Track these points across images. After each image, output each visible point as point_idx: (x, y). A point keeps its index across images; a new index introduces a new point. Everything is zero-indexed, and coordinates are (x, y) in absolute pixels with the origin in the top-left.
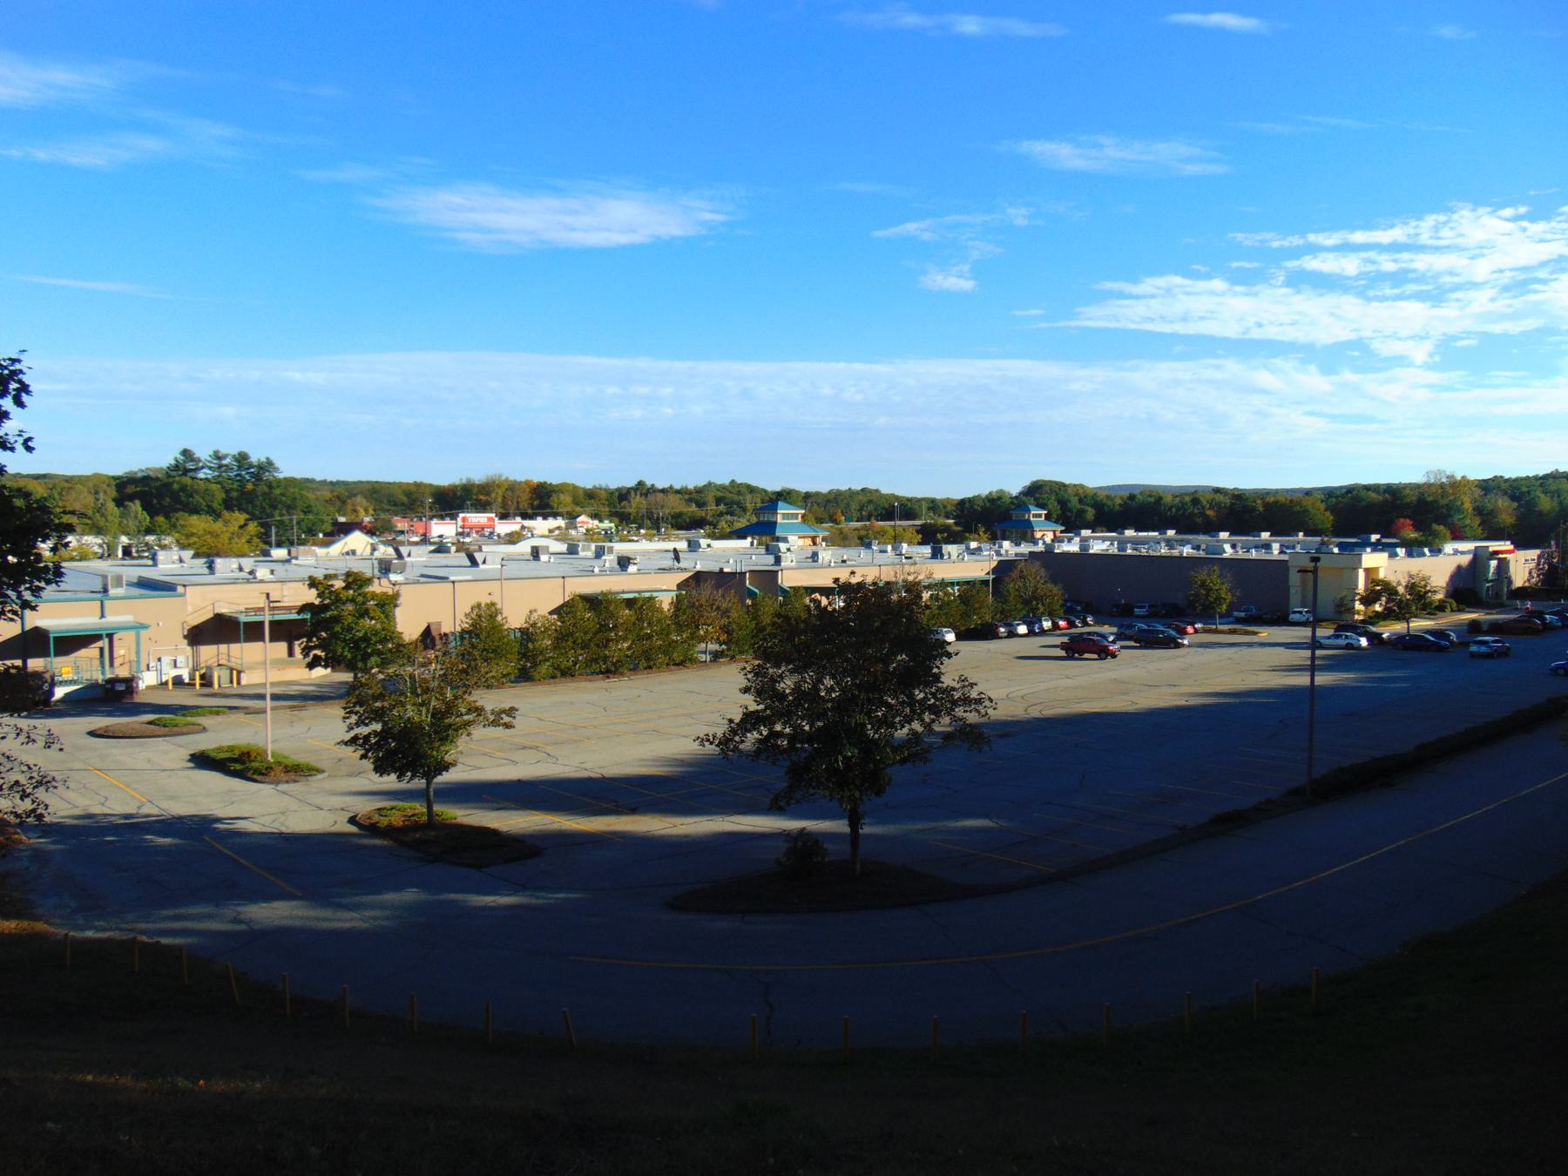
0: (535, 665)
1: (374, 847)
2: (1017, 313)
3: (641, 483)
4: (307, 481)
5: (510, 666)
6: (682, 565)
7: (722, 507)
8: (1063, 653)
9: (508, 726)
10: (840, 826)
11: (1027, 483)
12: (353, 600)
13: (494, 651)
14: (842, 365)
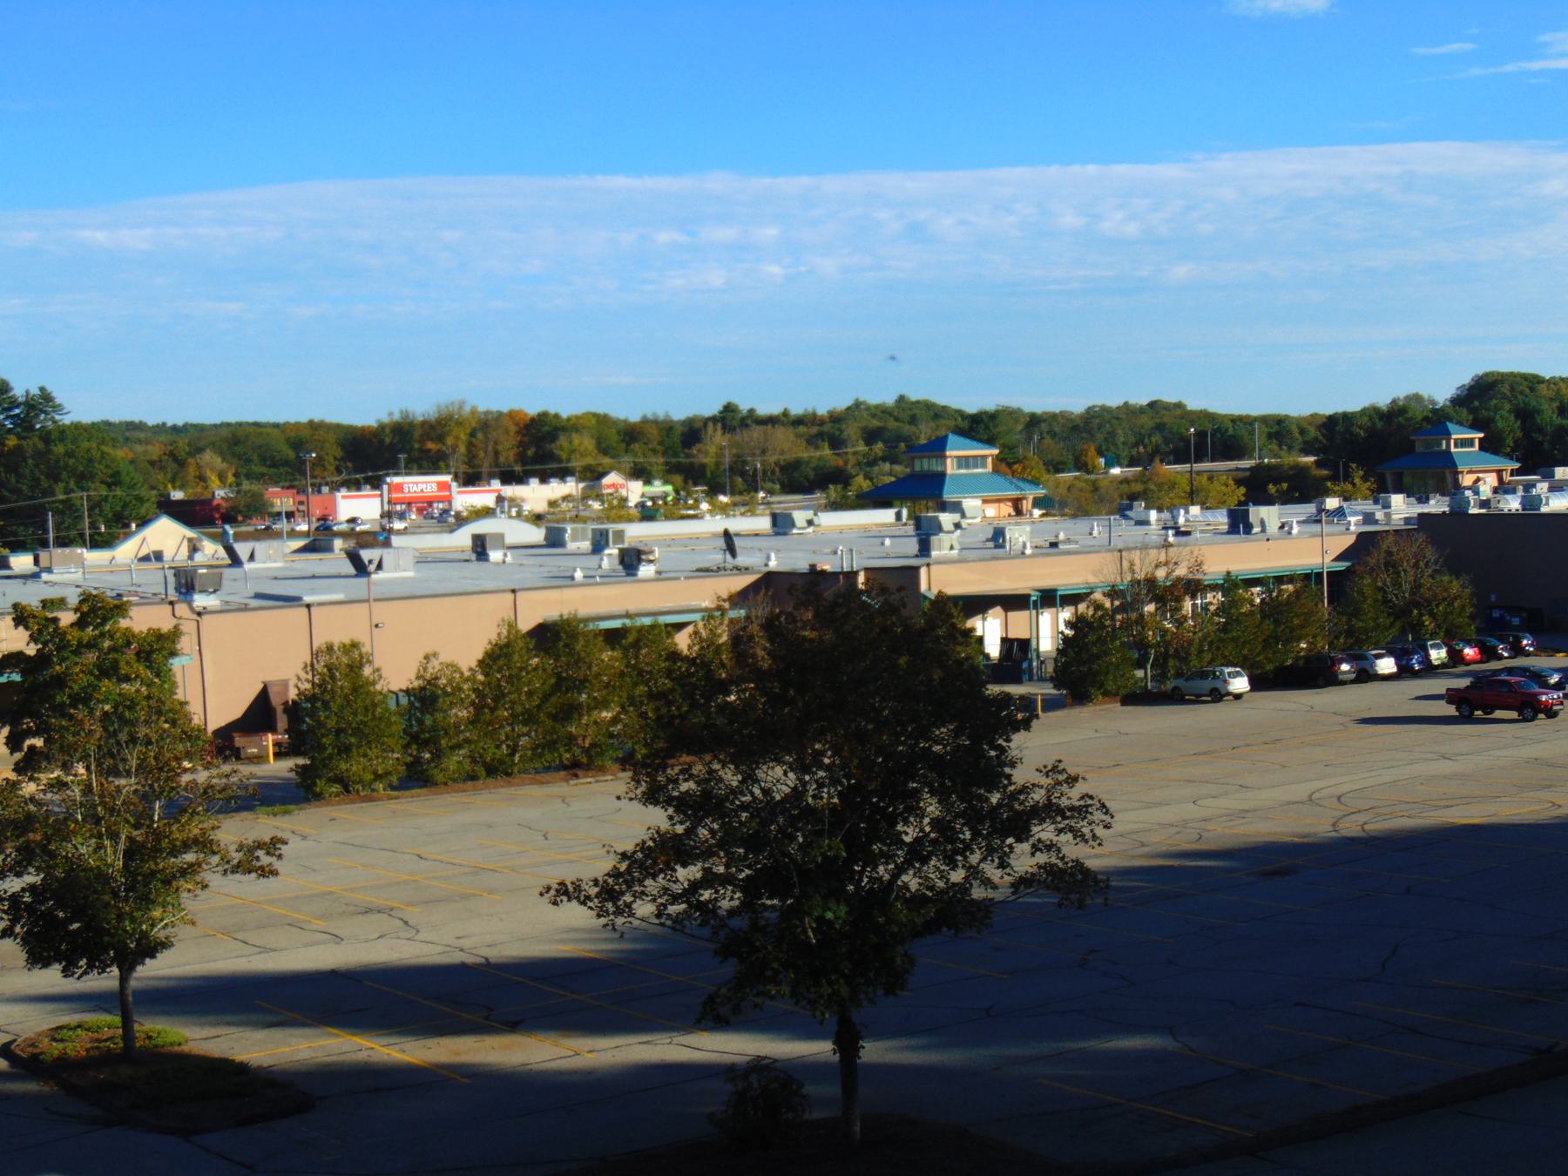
0: (438, 755)
1: (24, 1097)
2: (1422, 51)
3: (729, 409)
4: (131, 426)
5: (394, 759)
6: (742, 560)
7: (879, 447)
8: (1451, 710)
9: (266, 872)
10: (821, 1049)
11: (1466, 379)
12: (92, 645)
13: (357, 732)
14: (1092, 169)
